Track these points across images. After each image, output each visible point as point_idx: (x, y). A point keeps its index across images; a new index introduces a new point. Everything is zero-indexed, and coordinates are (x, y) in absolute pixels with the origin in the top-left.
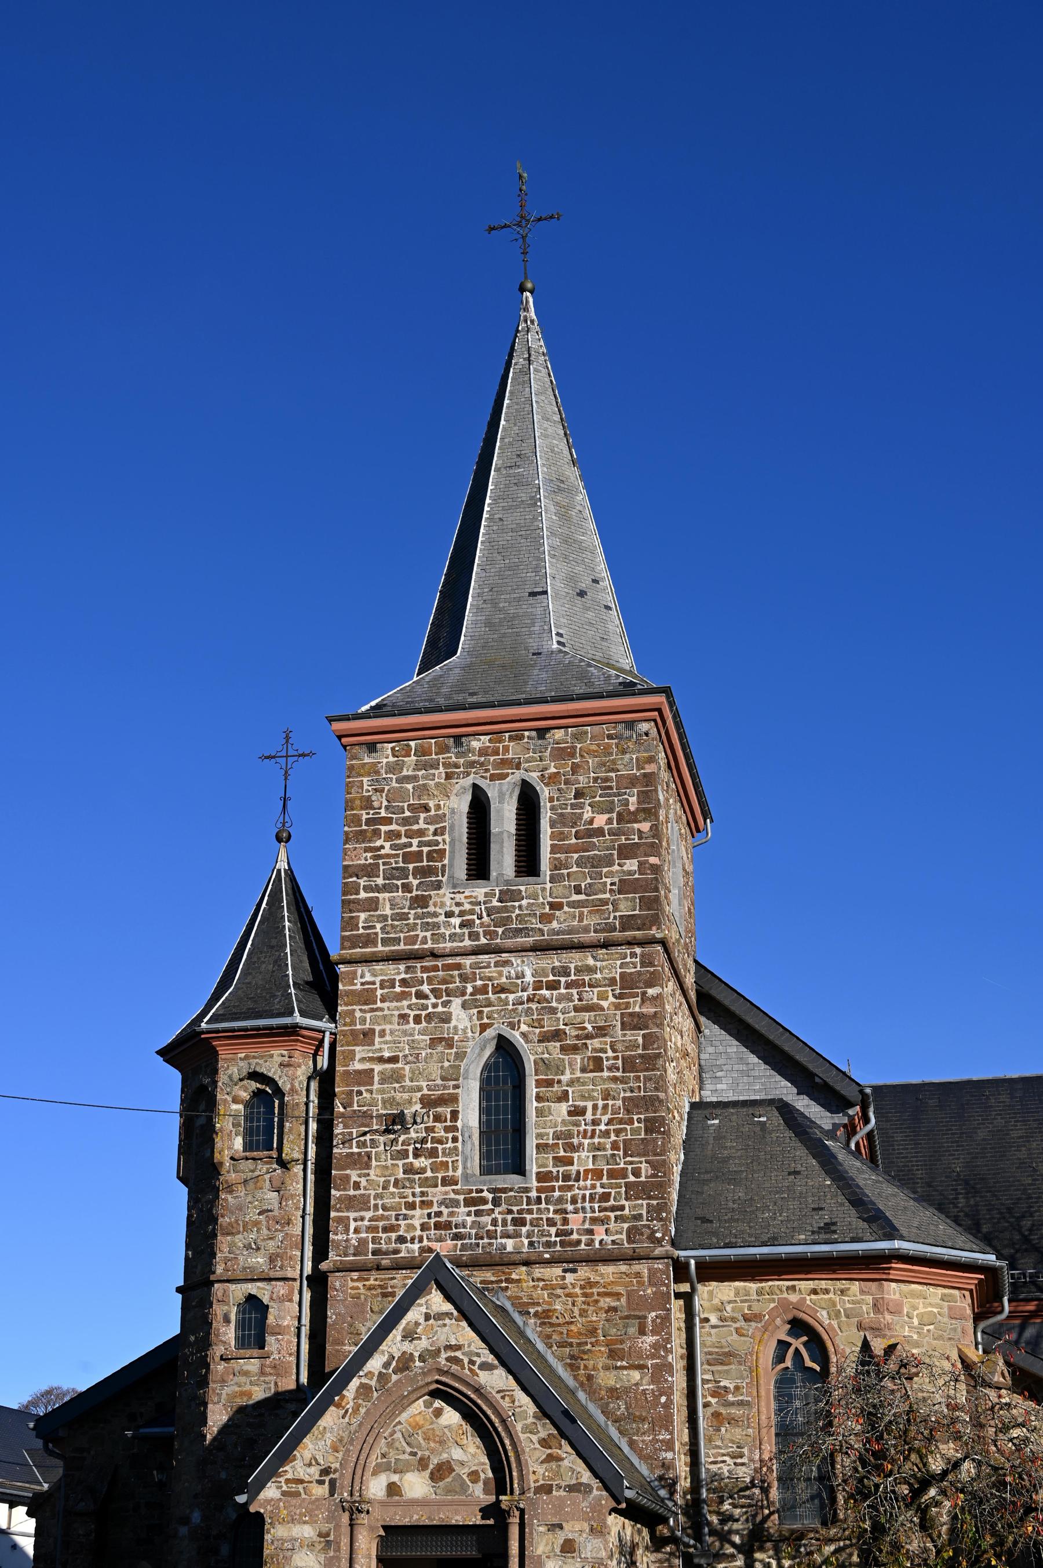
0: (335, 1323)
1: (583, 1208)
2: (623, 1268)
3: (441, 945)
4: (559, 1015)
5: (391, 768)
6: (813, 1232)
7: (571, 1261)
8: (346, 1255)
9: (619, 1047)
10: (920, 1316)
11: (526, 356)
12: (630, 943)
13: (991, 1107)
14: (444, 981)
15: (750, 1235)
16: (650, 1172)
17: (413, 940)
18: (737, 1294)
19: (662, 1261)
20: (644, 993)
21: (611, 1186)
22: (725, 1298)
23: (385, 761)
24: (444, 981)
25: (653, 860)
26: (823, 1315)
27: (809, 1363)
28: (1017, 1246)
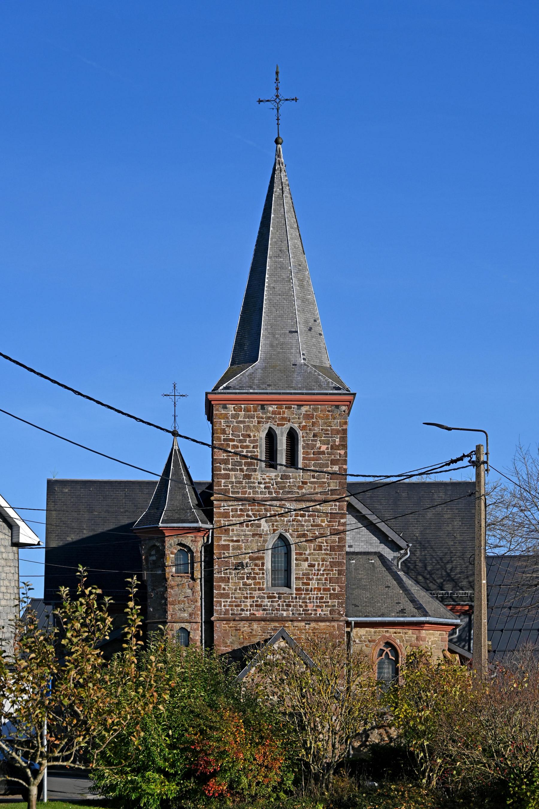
0: (217, 639)
1: (313, 602)
2: (328, 624)
3: (257, 496)
4: (305, 527)
5: (235, 416)
6: (397, 613)
7: (308, 621)
8: (220, 615)
9: (329, 541)
10: (432, 642)
11: (281, 187)
12: (335, 501)
13: (434, 499)
14: (258, 511)
15: (374, 613)
16: (339, 590)
17: (245, 493)
18: (367, 632)
20: (339, 521)
21: (324, 594)
22: (362, 634)
23: (231, 413)
24: (258, 511)
25: (344, 466)
26: (398, 641)
27: (391, 657)
28: (444, 578)
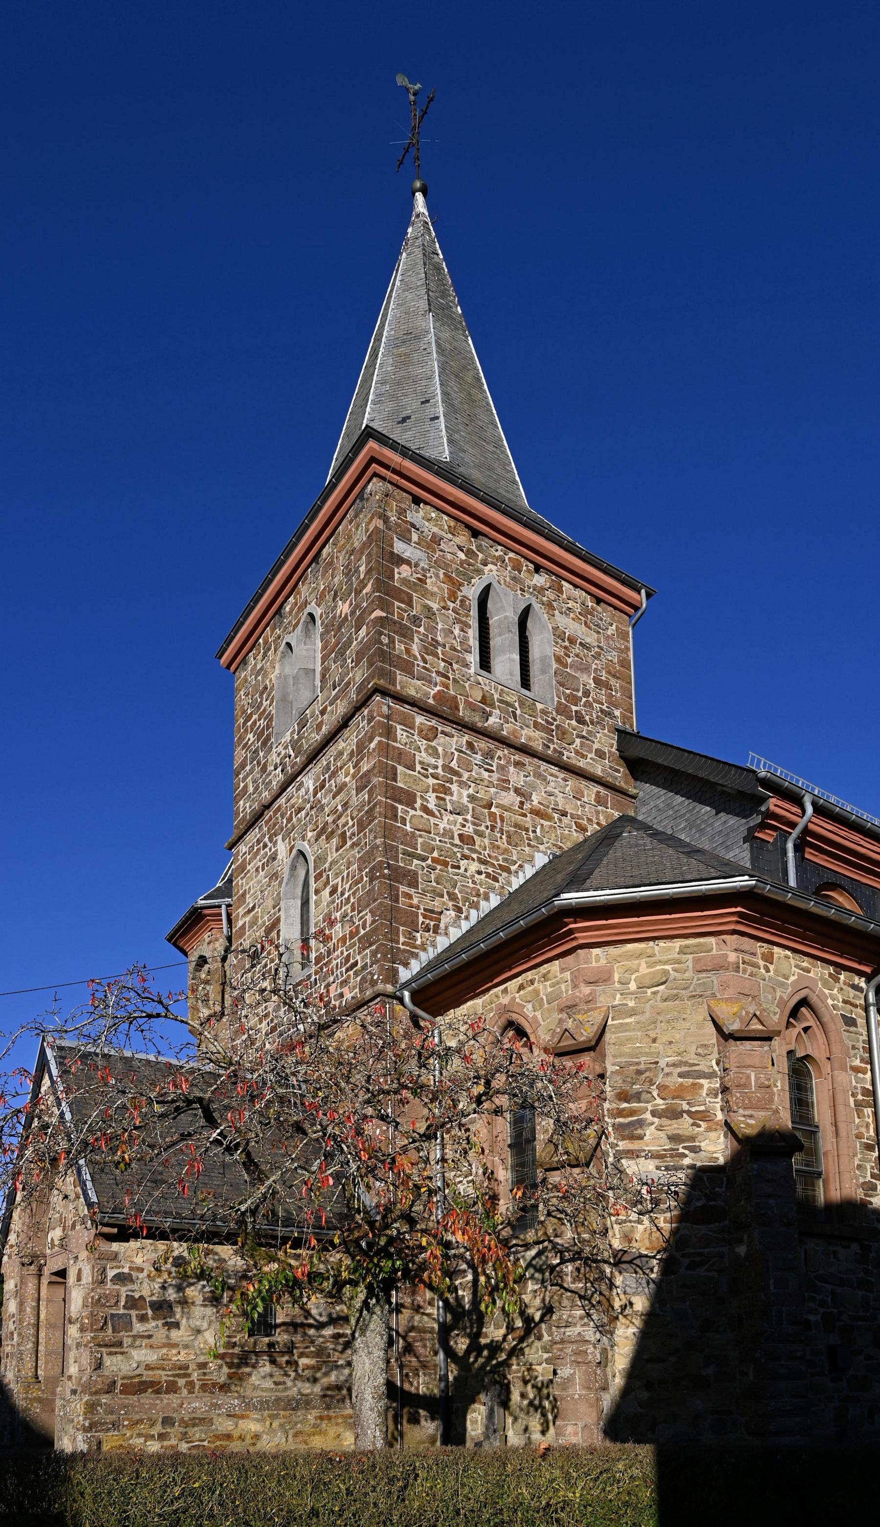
19: (376, 1001)
